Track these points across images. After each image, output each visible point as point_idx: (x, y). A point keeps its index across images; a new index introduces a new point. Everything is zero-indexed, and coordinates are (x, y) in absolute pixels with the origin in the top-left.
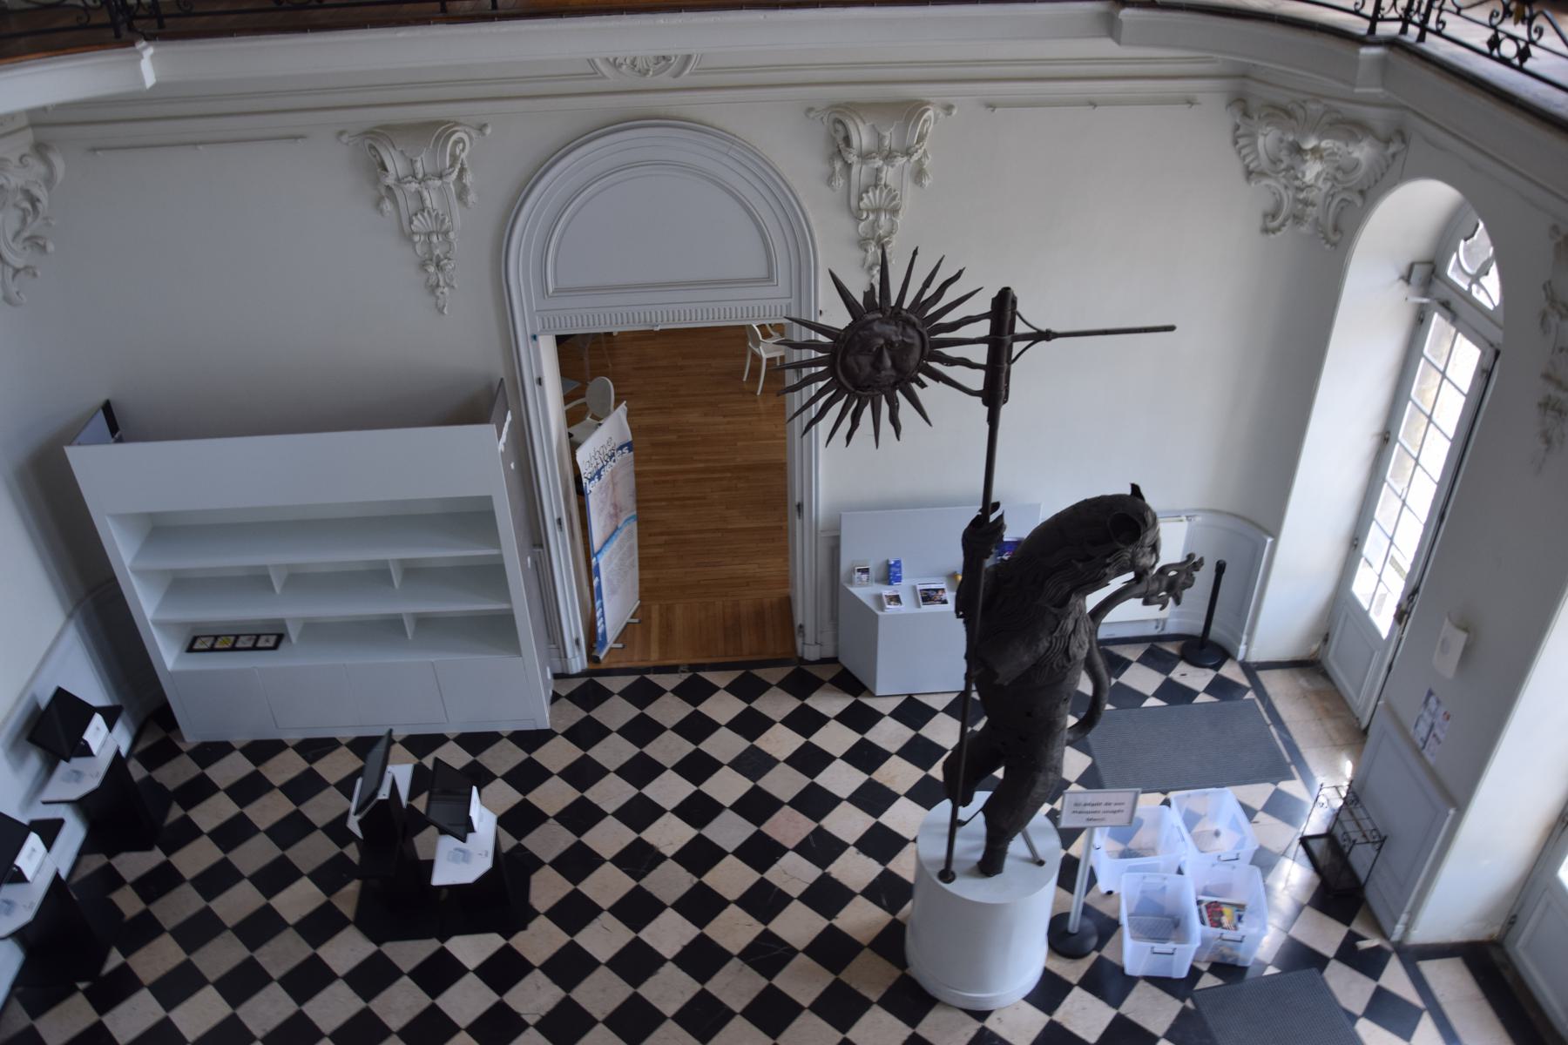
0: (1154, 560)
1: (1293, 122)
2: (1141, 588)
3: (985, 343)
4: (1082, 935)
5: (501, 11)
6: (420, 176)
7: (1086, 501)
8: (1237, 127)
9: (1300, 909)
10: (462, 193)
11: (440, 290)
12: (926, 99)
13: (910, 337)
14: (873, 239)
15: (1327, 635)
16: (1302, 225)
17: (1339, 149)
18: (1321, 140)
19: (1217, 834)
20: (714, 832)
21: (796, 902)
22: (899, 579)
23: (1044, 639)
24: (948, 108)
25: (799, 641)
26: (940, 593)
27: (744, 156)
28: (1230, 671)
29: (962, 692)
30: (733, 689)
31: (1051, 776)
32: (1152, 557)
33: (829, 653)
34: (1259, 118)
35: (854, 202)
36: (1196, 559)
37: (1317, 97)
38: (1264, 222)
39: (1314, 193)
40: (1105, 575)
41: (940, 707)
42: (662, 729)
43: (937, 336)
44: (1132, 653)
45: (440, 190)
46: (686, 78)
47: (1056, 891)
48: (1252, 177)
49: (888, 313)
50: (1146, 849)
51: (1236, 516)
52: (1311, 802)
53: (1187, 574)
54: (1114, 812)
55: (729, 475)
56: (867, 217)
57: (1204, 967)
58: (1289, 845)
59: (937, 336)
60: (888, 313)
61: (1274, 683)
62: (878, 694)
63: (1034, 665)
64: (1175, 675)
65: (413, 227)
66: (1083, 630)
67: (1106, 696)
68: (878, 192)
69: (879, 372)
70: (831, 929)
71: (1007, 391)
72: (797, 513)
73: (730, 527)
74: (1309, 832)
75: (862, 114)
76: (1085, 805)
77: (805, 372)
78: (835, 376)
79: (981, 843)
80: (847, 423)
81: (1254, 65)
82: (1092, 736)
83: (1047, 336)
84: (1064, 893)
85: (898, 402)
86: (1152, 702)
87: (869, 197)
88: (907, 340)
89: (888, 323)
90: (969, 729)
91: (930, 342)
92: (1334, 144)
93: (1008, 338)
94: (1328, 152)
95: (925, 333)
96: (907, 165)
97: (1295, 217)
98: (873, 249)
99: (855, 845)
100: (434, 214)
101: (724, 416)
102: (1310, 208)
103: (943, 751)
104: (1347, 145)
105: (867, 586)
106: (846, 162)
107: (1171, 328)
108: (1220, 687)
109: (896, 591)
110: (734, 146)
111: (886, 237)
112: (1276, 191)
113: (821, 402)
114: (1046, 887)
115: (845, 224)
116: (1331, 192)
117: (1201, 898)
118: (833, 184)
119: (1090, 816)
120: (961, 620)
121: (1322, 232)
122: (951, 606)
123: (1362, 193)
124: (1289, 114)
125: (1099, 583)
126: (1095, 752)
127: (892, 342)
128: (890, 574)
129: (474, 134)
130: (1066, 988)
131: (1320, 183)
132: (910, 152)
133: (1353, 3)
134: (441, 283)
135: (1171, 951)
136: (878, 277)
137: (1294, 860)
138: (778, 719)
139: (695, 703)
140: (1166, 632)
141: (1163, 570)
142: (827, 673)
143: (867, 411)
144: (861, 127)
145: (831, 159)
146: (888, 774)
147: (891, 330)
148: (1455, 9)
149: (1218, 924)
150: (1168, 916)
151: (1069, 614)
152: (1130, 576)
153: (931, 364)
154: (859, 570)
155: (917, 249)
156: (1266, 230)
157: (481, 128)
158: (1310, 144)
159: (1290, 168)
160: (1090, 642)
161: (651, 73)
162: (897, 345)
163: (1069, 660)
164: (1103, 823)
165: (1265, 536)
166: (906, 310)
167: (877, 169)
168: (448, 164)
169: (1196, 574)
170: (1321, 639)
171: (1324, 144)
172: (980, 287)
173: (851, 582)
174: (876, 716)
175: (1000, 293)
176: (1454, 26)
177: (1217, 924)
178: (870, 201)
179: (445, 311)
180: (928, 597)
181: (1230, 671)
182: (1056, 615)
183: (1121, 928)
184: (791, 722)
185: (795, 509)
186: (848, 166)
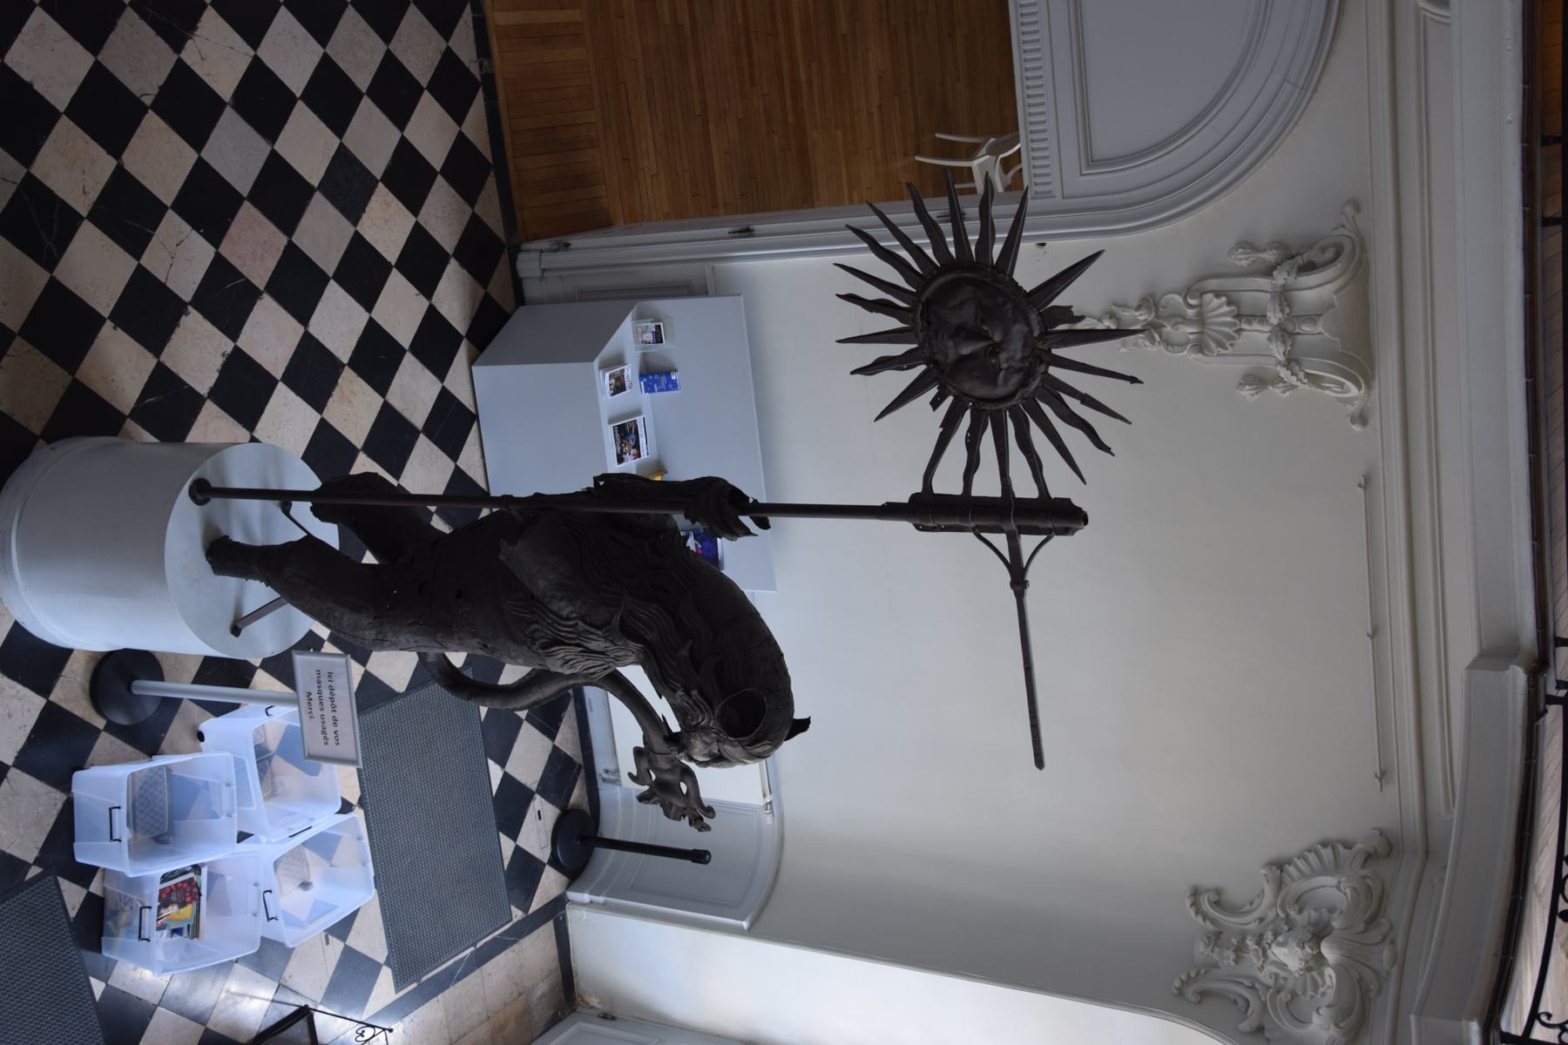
0: (701, 759)
1: (1361, 926)
2: (659, 744)
3: (1003, 491)
4: (131, 702)
7: (780, 655)
8: (1348, 846)
9: (199, 1019)
12: (1376, 383)
13: (1006, 380)
14: (1156, 316)
15: (613, 1018)
16: (1207, 946)
17: (1323, 994)
19: (305, 885)
20: (232, 126)
21: (134, 263)
22: (649, 389)
23: (571, 608)
24: (1362, 418)
25: (544, 244)
26: (633, 451)
28: (550, 883)
29: (489, 494)
30: (462, 145)
31: (370, 634)
32: (704, 755)
33: (531, 290)
34: (1365, 877)
35: (1214, 284)
36: (706, 820)
37: (1400, 961)
38: (1208, 890)
40: (675, 691)
41: (462, 462)
42: (387, 36)
43: (1009, 420)
44: (566, 738)
47: (200, 656)
49: (1040, 345)
50: (273, 783)
51: (779, 862)
52: (363, 1018)
53: (685, 809)
54: (324, 732)
55: (790, 120)
56: (1191, 306)
57: (95, 887)
58: (296, 993)
59: (1009, 420)
60: (1040, 345)
61: (537, 948)
62: (473, 368)
63: (533, 596)
64: (538, 803)
66: (590, 663)
67: (497, 705)
68: (1229, 319)
69: (952, 337)
70: (96, 321)
71: (933, 529)
72: (738, 228)
73: (711, 126)
74: (318, 1018)
76: (331, 688)
77: (946, 227)
78: (941, 271)
79: (259, 540)
80: (872, 293)
81: (1445, 867)
82: (436, 690)
83: (1019, 582)
84: (194, 669)
85: (908, 368)
86: (496, 773)
87: (1220, 306)
88: (1002, 374)
89: (1024, 346)
90: (433, 508)
91: (1000, 410)
92: (1329, 987)
93: (1013, 526)
96: (1273, 361)
97: (1218, 935)
98: (1143, 317)
99: (237, 350)
101: (880, 107)
102: (1232, 956)
103: (397, 472)
104: (1329, 1006)
105: (636, 338)
106: (1274, 267)
107: (1039, 762)
108: (525, 870)
109: (630, 387)
110: (1298, 90)
111: (1161, 337)
112: (1254, 905)
113: (904, 254)
114: (199, 642)
115: (1178, 272)
116: (1257, 985)
117: (204, 871)
118: (1240, 250)
119: (315, 696)
120: (591, 485)
121: (1198, 973)
122: (614, 468)
123: (1260, 1030)
124: (1372, 920)
125: (662, 683)
126: (414, 696)
127: (999, 353)
128: (656, 375)
130: (42, 686)
131: (1270, 969)
132: (1293, 364)
133: (1550, 1011)
135: (116, 836)
136: (1100, 326)
137: (273, 1001)
138: (422, 219)
139: (433, 88)
140: (601, 785)
141: (688, 774)
142: (499, 288)
143: (891, 323)
144: (1329, 288)
145: (1279, 244)
146: (352, 392)
147: (1014, 351)
149: (165, 902)
150: (171, 825)
151: (612, 642)
152: (675, 726)
153: (968, 414)
154: (658, 327)
155: (1141, 382)
156: (1196, 893)
160: (573, 676)
162: (993, 361)
163: (545, 647)
164: (306, 717)
165: (748, 919)
166: (1046, 372)
167: (1265, 316)
169: (686, 821)
170: (606, 1009)
171: (1329, 972)
172: (1087, 481)
173: (640, 317)
174: (440, 370)
175: (1066, 502)
177: (165, 902)
178: (1214, 310)
180: (626, 434)
181: (550, 883)
182: (609, 623)
183: (149, 759)
184: (419, 241)
185: (744, 225)
186: (1268, 272)
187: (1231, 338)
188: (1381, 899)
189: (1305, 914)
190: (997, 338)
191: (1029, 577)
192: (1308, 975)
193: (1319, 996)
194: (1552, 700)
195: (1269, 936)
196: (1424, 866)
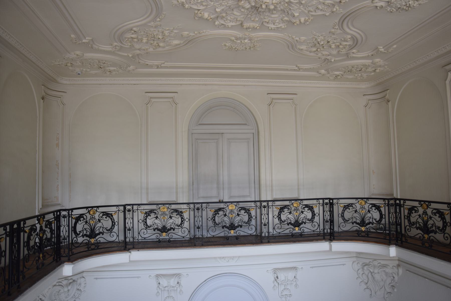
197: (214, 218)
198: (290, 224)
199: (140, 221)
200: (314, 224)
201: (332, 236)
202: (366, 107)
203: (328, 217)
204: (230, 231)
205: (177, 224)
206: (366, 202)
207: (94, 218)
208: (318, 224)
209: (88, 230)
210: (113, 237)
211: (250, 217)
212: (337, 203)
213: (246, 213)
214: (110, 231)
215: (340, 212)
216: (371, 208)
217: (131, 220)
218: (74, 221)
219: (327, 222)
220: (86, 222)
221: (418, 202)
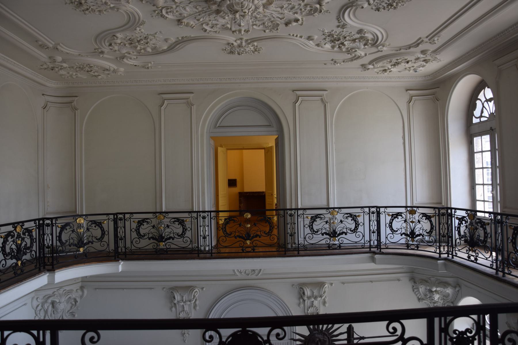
5: (213, 257)
6: (184, 301)
8: (413, 286)
10: (195, 307)
11: (185, 335)
12: (325, 282)
13: (326, 339)
18: (437, 288)
24: (331, 284)
27: (275, 298)
34: (419, 283)
37: (433, 276)
39: (438, 304)
45: (189, 305)
46: (259, 276)
48: (420, 300)
49: (319, 332)
60: (319, 332)
65: (180, 316)
68: (313, 308)
75: (308, 286)
87: (310, 310)
88: (324, 339)
89: (319, 334)
92: (441, 289)
93: (352, 339)
94: (440, 291)
95: (329, 337)
100: (186, 312)
104: (444, 289)
110: (272, 295)
112: (428, 304)
116: (444, 303)
124: (427, 281)
129: (200, 290)
132: (321, 296)
134: (186, 333)
145: (299, 299)
147: (320, 336)
148: (458, 250)
157: (202, 288)
158: (434, 289)
159: (430, 297)
161: (250, 275)
166: (324, 331)
168: (192, 298)
176: (459, 254)
178: (311, 311)
179: (186, 342)
186: (304, 301)
187: (316, 308)
188: (423, 280)
189: (428, 294)
190: (318, 339)
191: (362, 336)
192: (439, 293)
193: (443, 291)
194: (380, 251)
195: (433, 301)
196: (415, 273)
197: (271, 228)
198: (325, 235)
199: (133, 230)
200: (357, 234)
201: (379, 248)
202: (44, 108)
203: (374, 228)
204: (159, 243)
205: (177, 233)
206: (165, 216)
207: (414, 218)
208: (190, 240)
209: (75, 239)
210: (103, 246)
211: (311, 227)
212: (109, 218)
213: (353, 221)
214: (100, 241)
215: (388, 222)
216: (90, 226)
217: (123, 229)
218: (59, 230)
219: (374, 232)
220: (73, 231)
221: (465, 211)
